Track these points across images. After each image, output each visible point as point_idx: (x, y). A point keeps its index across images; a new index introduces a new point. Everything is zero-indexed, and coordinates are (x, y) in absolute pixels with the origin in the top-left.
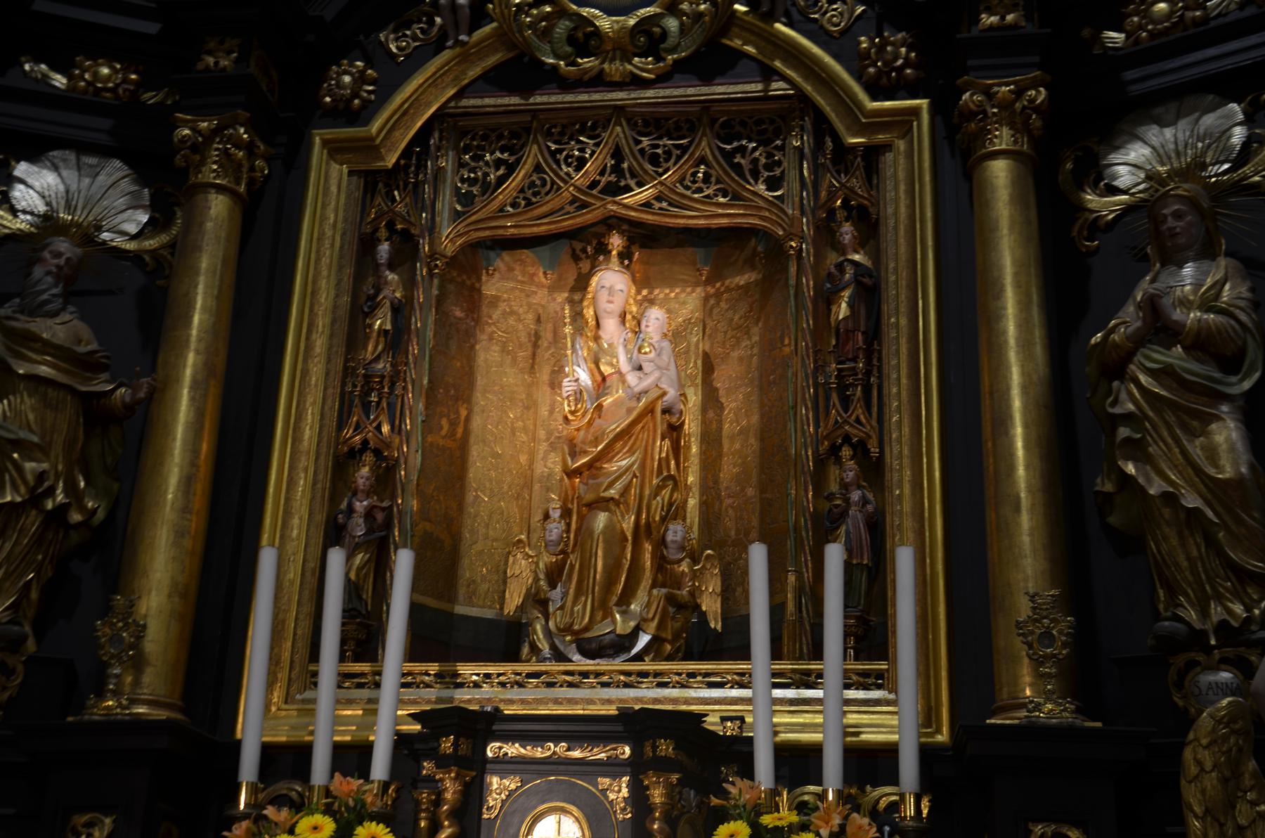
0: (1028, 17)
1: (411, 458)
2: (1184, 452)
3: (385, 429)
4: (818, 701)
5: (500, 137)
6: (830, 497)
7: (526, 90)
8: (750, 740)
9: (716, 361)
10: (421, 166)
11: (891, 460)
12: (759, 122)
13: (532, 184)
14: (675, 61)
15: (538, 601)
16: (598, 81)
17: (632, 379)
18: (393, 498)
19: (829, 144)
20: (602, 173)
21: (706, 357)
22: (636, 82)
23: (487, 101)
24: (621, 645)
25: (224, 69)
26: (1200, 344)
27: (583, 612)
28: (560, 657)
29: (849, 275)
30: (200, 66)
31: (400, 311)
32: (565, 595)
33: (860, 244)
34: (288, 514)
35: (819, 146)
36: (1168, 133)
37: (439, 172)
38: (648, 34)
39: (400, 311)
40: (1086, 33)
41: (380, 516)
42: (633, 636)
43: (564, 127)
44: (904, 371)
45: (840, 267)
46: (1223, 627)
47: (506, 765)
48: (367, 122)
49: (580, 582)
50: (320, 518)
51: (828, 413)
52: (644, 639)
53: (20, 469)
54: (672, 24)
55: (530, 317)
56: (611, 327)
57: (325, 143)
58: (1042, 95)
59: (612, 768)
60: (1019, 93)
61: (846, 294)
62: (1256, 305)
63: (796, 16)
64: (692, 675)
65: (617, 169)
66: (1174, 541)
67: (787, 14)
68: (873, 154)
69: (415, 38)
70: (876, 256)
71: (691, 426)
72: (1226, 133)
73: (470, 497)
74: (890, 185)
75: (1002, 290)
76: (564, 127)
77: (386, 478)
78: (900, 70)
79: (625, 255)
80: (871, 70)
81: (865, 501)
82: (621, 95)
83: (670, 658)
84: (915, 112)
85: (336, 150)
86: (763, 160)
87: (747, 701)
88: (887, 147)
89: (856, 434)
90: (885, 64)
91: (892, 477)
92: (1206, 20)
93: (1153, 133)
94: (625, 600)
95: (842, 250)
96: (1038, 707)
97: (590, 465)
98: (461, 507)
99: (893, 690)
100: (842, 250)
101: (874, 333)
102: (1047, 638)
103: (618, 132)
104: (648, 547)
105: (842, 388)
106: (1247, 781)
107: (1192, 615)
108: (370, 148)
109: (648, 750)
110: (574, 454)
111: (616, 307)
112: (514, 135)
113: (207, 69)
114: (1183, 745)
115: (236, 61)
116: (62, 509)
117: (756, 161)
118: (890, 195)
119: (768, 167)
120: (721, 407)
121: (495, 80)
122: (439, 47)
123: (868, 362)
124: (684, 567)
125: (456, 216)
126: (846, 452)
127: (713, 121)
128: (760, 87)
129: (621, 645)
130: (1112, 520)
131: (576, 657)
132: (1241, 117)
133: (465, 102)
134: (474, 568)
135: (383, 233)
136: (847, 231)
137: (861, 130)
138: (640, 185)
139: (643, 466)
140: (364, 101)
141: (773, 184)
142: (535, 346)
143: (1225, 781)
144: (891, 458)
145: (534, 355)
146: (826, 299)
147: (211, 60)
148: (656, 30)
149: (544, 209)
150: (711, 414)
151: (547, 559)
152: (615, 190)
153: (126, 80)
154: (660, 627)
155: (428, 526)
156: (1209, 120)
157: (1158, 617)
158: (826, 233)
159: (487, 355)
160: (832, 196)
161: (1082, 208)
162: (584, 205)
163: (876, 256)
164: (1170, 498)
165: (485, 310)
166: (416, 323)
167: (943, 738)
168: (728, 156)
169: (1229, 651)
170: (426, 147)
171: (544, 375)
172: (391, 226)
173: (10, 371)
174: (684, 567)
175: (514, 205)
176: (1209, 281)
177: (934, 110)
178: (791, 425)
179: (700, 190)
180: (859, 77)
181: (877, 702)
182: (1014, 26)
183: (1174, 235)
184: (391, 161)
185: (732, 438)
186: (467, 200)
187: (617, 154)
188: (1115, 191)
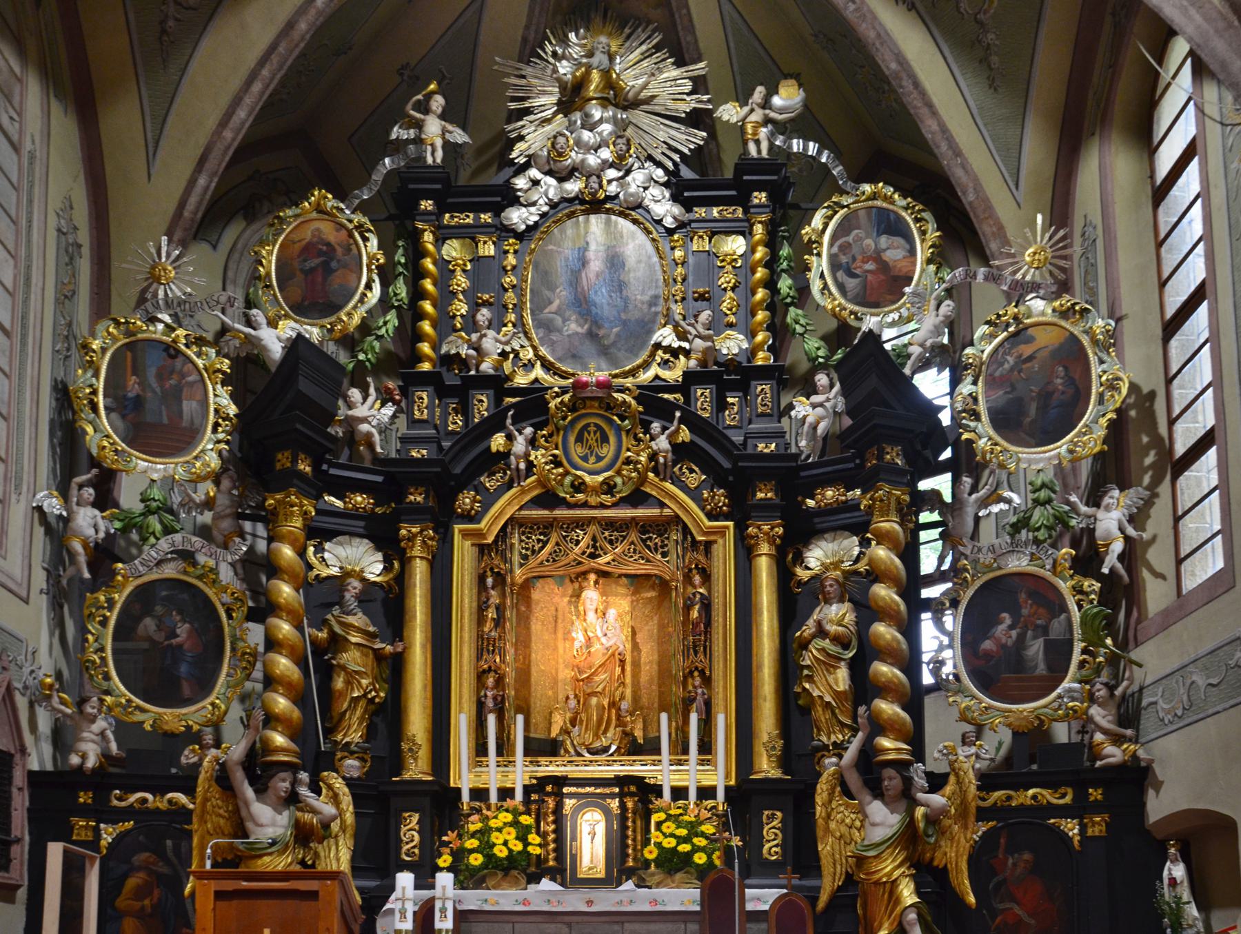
0: (776, 495)
1: (510, 673)
2: (826, 680)
3: (498, 660)
4: (688, 771)
5: (539, 528)
6: (690, 692)
7: (551, 507)
8: (661, 785)
9: (637, 630)
10: (504, 541)
11: (714, 676)
12: (658, 525)
13: (555, 552)
14: (621, 498)
16: (585, 505)
17: (604, 640)
18: (504, 690)
19: (689, 539)
20: (588, 548)
21: (633, 628)
22: (602, 506)
23: (534, 512)
24: (605, 750)
25: (419, 503)
26: (836, 639)
27: (589, 737)
28: (579, 754)
29: (698, 596)
30: (408, 500)
31: (500, 609)
32: (580, 730)
33: (703, 584)
34: (461, 698)
35: (685, 538)
36: (830, 545)
37: (512, 545)
38: (608, 484)
39: (500, 609)
40: (799, 499)
41: (499, 698)
42: (609, 747)
43: (569, 524)
44: (721, 641)
45: (694, 594)
46: (835, 743)
47: (571, 796)
48: (479, 522)
49: (587, 725)
50: (474, 699)
51: (688, 657)
52: (613, 748)
53: (359, 683)
54: (619, 480)
55: (553, 608)
56: (591, 616)
57: (460, 531)
58: (780, 531)
59: (612, 796)
60: (772, 529)
61: (697, 607)
62: (857, 623)
63: (675, 479)
64: (634, 761)
65: (594, 546)
66: (821, 712)
67: (671, 478)
68: (708, 545)
69: (498, 481)
70: (709, 591)
71: (628, 659)
72: (851, 549)
73: (533, 689)
74: (716, 559)
75: (762, 613)
76: (569, 524)
77: (500, 682)
78: (721, 507)
79: (596, 582)
80: (709, 507)
81: (703, 694)
82: (596, 512)
83: (623, 755)
84: (727, 527)
85: (466, 534)
86: (660, 544)
87: (660, 771)
88: (715, 542)
89: (700, 666)
90: (715, 504)
91: (714, 684)
92: (847, 501)
93: (823, 544)
94: (605, 732)
95: (695, 587)
96: (769, 772)
97: (587, 678)
98: (530, 693)
99: (716, 767)
100: (695, 587)
101: (708, 624)
102: (774, 748)
103: (593, 529)
104: (614, 711)
105: (695, 647)
106: (837, 794)
107: (824, 739)
108: (480, 534)
109: (626, 789)
110: (581, 672)
111: (594, 607)
112: (545, 527)
113: (411, 502)
114: (817, 783)
115: (424, 498)
116: (374, 697)
117: (656, 544)
118: (716, 564)
119: (662, 547)
120: (640, 651)
121: (537, 502)
122: (510, 487)
123: (705, 636)
124: (628, 719)
125: (521, 565)
126: (696, 674)
127: (637, 524)
128: (659, 511)
129: (605, 750)
130: (800, 702)
131: (587, 755)
132: (857, 543)
133: (523, 512)
134: (536, 718)
135: (489, 573)
136: (697, 579)
137: (705, 534)
138: (605, 554)
139: (610, 679)
140: (477, 511)
141: (664, 555)
142: (556, 621)
143: (829, 794)
144: (297, 46)
145: (556, 626)
146: (688, 608)
147: (412, 498)
148: (612, 483)
149: (562, 564)
150: (635, 654)
151: (569, 715)
152: (593, 556)
153: (369, 503)
154: (620, 743)
155: (518, 702)
156: (846, 542)
157: (813, 739)
158: (688, 579)
159: (536, 627)
160: (690, 563)
161: (794, 575)
162: (580, 563)
163: (709, 591)
164: (821, 697)
165: (533, 606)
166: (508, 614)
167: (732, 783)
168: (644, 541)
169: (836, 751)
170: (505, 533)
171: (560, 635)
172: (492, 569)
173: (347, 640)
174: (628, 719)
175: (548, 561)
176: (841, 614)
177: (736, 527)
178: (673, 662)
179: (632, 557)
180: (703, 509)
181: (707, 771)
182: (770, 499)
183: (829, 593)
184: (490, 540)
185: (645, 664)
186: (525, 557)
187: (594, 539)
188: (808, 568)
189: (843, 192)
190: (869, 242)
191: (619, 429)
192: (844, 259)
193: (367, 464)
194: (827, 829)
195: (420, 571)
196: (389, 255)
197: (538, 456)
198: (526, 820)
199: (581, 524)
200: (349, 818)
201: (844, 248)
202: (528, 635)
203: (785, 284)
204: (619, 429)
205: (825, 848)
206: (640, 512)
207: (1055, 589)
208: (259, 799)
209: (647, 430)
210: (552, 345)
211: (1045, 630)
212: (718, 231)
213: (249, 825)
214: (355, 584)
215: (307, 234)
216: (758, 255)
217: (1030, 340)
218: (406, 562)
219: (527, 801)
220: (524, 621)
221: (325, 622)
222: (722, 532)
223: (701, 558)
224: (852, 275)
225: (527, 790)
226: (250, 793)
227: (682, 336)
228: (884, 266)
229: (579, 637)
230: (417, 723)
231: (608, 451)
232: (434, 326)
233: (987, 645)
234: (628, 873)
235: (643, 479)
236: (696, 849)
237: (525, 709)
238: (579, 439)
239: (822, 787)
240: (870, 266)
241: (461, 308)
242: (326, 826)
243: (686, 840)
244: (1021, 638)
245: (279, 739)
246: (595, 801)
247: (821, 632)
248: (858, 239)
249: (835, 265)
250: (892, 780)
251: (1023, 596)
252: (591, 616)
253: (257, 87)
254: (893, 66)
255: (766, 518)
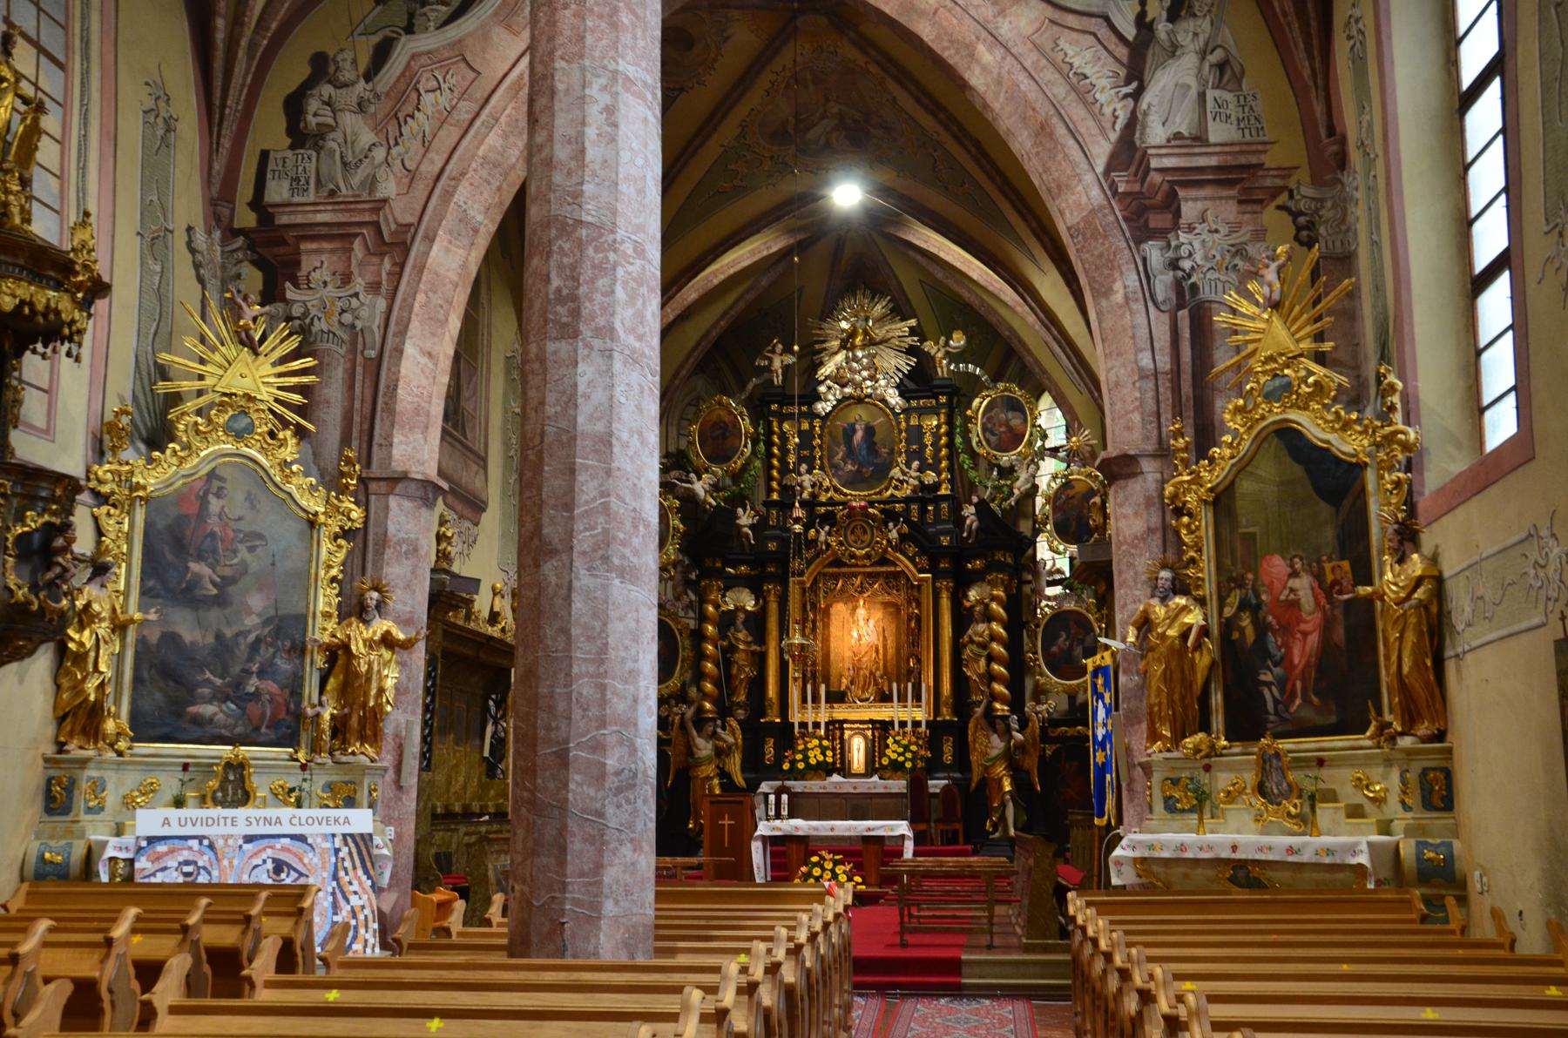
15: (847, 687)
16: (857, 566)
22: (865, 566)
24: (867, 700)
31: (814, 622)
56: (861, 623)
68: (919, 587)
101: (920, 630)
108: (803, 583)
129: (867, 700)
134: (833, 679)
189: (988, 389)
190: (1003, 416)
191: (871, 527)
192: (989, 426)
193: (748, 551)
194: (975, 748)
195: (773, 607)
196: (756, 427)
197: (833, 541)
198: (825, 743)
199: (855, 575)
200: (740, 741)
201: (989, 419)
202: (829, 636)
203: (958, 440)
204: (871, 527)
205: (974, 758)
206: (884, 569)
207: (1088, 619)
208: (700, 736)
209: (887, 527)
210: (839, 477)
211: (1082, 642)
212: (923, 412)
213: (695, 749)
214: (742, 616)
215: (714, 417)
216: (943, 430)
217: (1073, 487)
218: (766, 603)
219: (827, 730)
220: (826, 626)
221: (727, 636)
222: (926, 580)
223: (916, 594)
224: (993, 434)
225: (827, 724)
226: (695, 733)
227: (904, 474)
228: (1010, 429)
229: (855, 634)
230: (772, 691)
231: (867, 538)
232: (779, 473)
233: (1054, 649)
234: (875, 771)
235: (885, 551)
236: (906, 759)
237: (827, 680)
238: (853, 532)
239: (971, 725)
240: (1003, 429)
241: (792, 459)
242: (729, 748)
243: (902, 754)
244: (1071, 645)
245: (708, 705)
246: (861, 732)
247: (972, 641)
248: (997, 414)
249: (984, 429)
250: (1000, 725)
251: (1071, 623)
252: (861, 623)
253: (692, 360)
254: (1007, 333)
255: (944, 578)
